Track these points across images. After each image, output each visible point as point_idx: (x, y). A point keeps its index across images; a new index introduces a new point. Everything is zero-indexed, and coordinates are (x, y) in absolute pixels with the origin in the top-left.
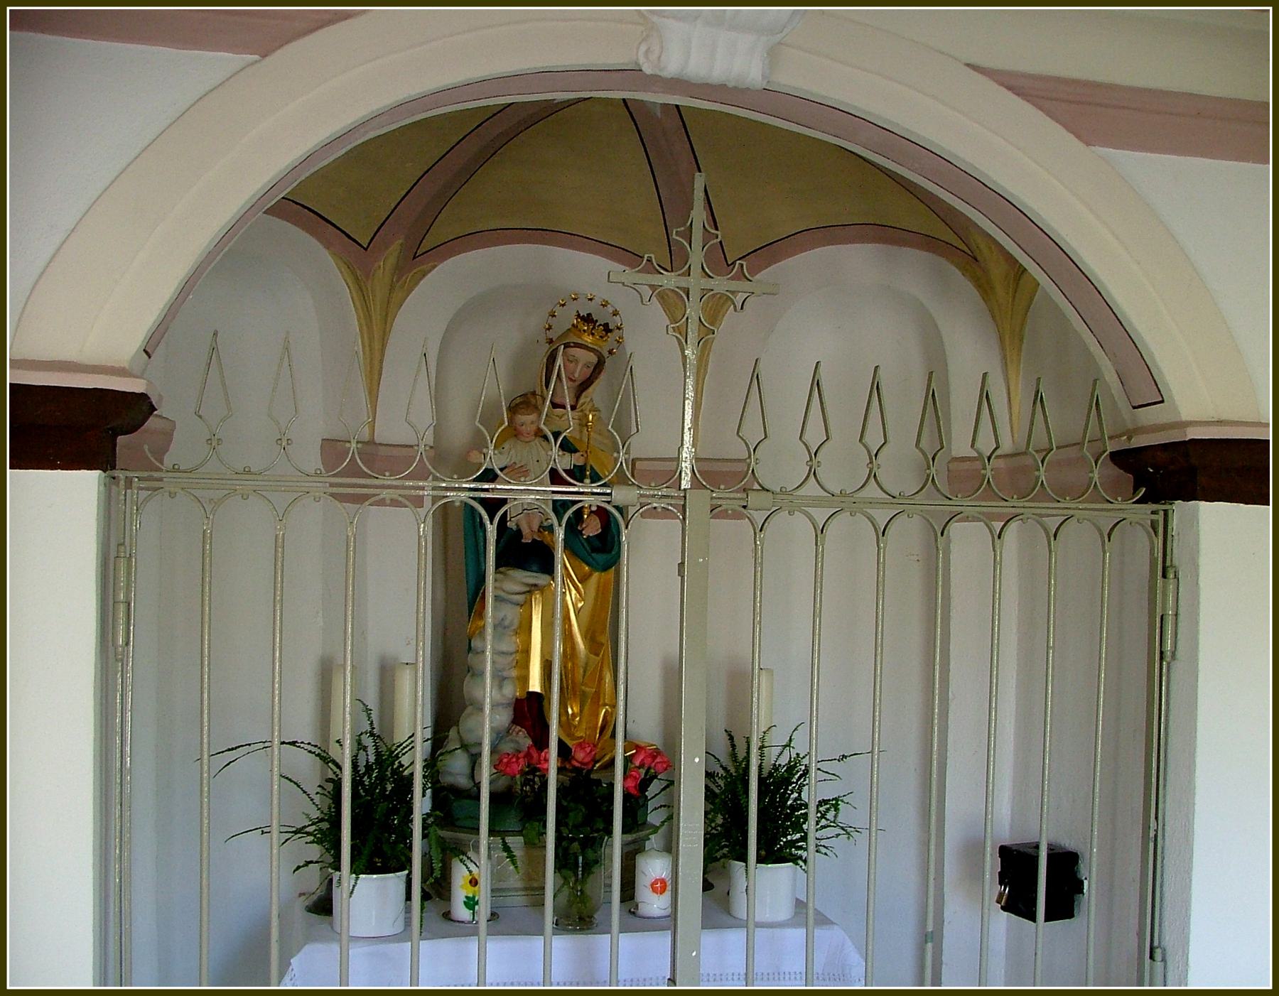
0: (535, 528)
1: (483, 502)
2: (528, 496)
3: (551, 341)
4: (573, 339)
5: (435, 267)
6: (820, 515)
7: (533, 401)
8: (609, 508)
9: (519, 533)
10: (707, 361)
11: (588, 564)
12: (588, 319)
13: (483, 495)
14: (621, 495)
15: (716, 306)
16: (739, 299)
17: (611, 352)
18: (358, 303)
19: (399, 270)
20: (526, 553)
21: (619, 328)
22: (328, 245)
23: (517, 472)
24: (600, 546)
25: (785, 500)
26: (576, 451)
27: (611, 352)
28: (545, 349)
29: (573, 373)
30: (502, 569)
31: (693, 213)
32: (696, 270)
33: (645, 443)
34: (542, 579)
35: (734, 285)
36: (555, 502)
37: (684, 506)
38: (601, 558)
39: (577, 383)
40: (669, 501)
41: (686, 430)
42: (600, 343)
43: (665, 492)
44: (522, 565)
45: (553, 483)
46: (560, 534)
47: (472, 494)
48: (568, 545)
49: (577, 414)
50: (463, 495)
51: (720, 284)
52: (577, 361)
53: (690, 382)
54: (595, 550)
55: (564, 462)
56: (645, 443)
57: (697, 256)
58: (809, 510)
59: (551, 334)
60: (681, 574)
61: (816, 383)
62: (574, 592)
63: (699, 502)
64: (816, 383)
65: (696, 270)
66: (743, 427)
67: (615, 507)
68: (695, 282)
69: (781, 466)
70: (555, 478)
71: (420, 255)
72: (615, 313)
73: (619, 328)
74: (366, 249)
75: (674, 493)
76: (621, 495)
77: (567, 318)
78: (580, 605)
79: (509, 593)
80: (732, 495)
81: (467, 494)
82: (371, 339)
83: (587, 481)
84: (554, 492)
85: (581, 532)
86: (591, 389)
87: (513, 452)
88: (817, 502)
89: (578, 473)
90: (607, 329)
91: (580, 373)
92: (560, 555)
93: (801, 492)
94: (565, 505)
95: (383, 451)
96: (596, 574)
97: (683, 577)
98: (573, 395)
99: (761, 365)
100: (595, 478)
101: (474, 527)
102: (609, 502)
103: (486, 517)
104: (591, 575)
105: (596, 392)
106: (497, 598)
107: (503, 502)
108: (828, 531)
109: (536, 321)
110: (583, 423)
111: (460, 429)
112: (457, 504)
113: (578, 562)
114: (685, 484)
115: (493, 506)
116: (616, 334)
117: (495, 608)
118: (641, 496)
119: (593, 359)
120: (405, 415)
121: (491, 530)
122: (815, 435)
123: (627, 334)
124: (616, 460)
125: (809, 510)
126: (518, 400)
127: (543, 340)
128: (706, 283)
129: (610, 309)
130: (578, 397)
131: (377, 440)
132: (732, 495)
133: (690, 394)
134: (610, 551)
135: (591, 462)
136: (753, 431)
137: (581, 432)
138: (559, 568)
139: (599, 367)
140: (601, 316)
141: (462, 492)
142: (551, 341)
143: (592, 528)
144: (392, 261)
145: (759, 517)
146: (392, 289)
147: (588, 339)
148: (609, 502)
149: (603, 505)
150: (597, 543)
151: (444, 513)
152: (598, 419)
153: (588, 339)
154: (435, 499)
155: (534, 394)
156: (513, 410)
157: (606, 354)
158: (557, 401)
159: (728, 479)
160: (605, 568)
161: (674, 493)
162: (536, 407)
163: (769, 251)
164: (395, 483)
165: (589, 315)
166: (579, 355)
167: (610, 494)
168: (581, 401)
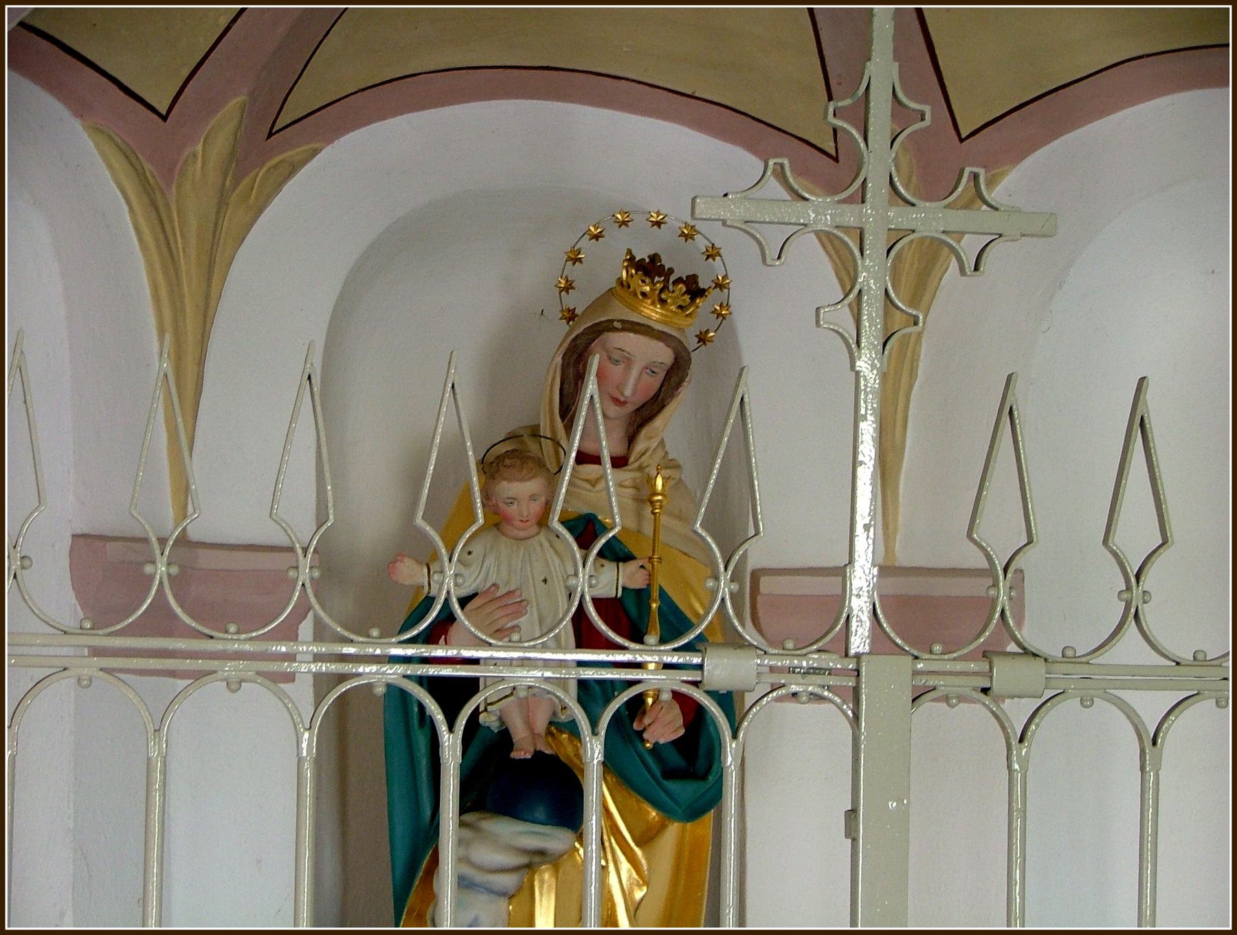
0: (541, 724)
1: (434, 685)
2: (528, 670)
3: (571, 316)
4: (619, 312)
5: (315, 152)
6: (1151, 705)
7: (532, 446)
8: (698, 695)
9: (504, 738)
10: (915, 361)
11: (656, 804)
12: (650, 267)
13: (432, 671)
14: (722, 669)
15: (920, 266)
16: (969, 247)
17: (702, 339)
18: (149, 238)
19: (241, 162)
20: (523, 782)
21: (720, 286)
22: (80, 109)
23: (500, 609)
24: (682, 766)
25: (1076, 675)
26: (628, 558)
27: (702, 339)
28: (557, 334)
29: (620, 387)
30: (468, 817)
31: (872, 68)
32: (877, 189)
33: (779, 540)
34: (555, 839)
35: (957, 219)
36: (582, 684)
37: (856, 691)
38: (684, 790)
39: (630, 408)
40: (819, 679)
41: (859, 530)
42: (680, 321)
43: (814, 660)
44: (509, 808)
45: (581, 644)
46: (594, 750)
47: (410, 670)
48: (610, 764)
49: (626, 475)
50: (394, 672)
51: (929, 218)
52: (629, 361)
53: (868, 429)
54: (671, 774)
55: (599, 581)
56: (779, 540)
57: (879, 159)
58: (1125, 695)
59: (571, 300)
60: (851, 831)
61: (1139, 424)
62: (625, 865)
63: (887, 680)
64: (1139, 424)
65: (877, 189)
66: (982, 523)
67: (709, 693)
68: (877, 215)
69: (1065, 607)
70: (585, 636)
71: (281, 129)
72: (712, 253)
73: (720, 286)
74: (165, 118)
75: (833, 662)
76: (722, 669)
77: (606, 266)
78: (639, 894)
79: (480, 868)
80: (959, 666)
81: (400, 669)
82: (178, 312)
83: (651, 639)
84: (581, 664)
85: (640, 734)
86: (658, 422)
87: (491, 560)
88: (1144, 679)
89: (627, 616)
90: (695, 291)
91: (635, 386)
92: (597, 792)
93: (1105, 658)
94: (608, 689)
95: (207, 560)
96: (674, 828)
97: (855, 840)
98: (619, 433)
99: (1019, 387)
100: (675, 624)
101: (407, 724)
102: (696, 684)
103: (439, 717)
104: (662, 828)
105: (671, 427)
106: (464, 883)
107: (472, 686)
108: (1170, 741)
109: (538, 270)
110: (644, 496)
111: (373, 510)
112: (380, 690)
113: (633, 800)
114: (859, 642)
115: (454, 693)
116: (714, 297)
117: (458, 905)
118: (772, 669)
119: (664, 355)
120: (259, 477)
121: (451, 744)
122: (1136, 533)
123: (737, 294)
124: (714, 592)
125: (1125, 695)
126: (502, 449)
127: (555, 312)
128: (899, 217)
129: (701, 243)
130: (631, 439)
131: (194, 534)
132: (959, 666)
133: (868, 451)
134: (704, 777)
135: (662, 580)
136: (1001, 532)
137: (639, 516)
138: (593, 822)
139: (676, 373)
140: (680, 262)
141: (386, 663)
142: (571, 316)
143: (664, 728)
144: (222, 142)
145: (1017, 711)
146: (222, 202)
147: (652, 313)
148: (696, 684)
149: (686, 689)
150: (675, 759)
151: (342, 718)
152: (676, 485)
153: (652, 313)
154: (323, 684)
155: (535, 433)
156: (491, 467)
157: (691, 343)
158: (590, 448)
159: (951, 620)
160: (694, 813)
161: (833, 662)
162: (540, 464)
163: (1051, 106)
164: (247, 647)
165: (654, 258)
166: (629, 346)
167: (700, 667)
168: (640, 446)
